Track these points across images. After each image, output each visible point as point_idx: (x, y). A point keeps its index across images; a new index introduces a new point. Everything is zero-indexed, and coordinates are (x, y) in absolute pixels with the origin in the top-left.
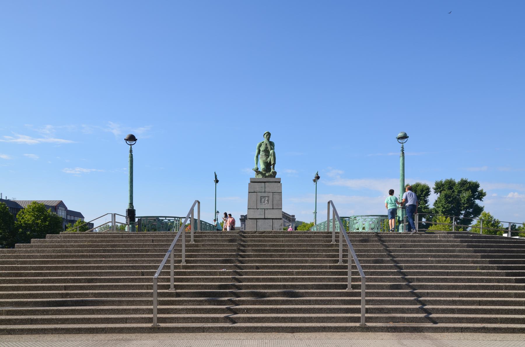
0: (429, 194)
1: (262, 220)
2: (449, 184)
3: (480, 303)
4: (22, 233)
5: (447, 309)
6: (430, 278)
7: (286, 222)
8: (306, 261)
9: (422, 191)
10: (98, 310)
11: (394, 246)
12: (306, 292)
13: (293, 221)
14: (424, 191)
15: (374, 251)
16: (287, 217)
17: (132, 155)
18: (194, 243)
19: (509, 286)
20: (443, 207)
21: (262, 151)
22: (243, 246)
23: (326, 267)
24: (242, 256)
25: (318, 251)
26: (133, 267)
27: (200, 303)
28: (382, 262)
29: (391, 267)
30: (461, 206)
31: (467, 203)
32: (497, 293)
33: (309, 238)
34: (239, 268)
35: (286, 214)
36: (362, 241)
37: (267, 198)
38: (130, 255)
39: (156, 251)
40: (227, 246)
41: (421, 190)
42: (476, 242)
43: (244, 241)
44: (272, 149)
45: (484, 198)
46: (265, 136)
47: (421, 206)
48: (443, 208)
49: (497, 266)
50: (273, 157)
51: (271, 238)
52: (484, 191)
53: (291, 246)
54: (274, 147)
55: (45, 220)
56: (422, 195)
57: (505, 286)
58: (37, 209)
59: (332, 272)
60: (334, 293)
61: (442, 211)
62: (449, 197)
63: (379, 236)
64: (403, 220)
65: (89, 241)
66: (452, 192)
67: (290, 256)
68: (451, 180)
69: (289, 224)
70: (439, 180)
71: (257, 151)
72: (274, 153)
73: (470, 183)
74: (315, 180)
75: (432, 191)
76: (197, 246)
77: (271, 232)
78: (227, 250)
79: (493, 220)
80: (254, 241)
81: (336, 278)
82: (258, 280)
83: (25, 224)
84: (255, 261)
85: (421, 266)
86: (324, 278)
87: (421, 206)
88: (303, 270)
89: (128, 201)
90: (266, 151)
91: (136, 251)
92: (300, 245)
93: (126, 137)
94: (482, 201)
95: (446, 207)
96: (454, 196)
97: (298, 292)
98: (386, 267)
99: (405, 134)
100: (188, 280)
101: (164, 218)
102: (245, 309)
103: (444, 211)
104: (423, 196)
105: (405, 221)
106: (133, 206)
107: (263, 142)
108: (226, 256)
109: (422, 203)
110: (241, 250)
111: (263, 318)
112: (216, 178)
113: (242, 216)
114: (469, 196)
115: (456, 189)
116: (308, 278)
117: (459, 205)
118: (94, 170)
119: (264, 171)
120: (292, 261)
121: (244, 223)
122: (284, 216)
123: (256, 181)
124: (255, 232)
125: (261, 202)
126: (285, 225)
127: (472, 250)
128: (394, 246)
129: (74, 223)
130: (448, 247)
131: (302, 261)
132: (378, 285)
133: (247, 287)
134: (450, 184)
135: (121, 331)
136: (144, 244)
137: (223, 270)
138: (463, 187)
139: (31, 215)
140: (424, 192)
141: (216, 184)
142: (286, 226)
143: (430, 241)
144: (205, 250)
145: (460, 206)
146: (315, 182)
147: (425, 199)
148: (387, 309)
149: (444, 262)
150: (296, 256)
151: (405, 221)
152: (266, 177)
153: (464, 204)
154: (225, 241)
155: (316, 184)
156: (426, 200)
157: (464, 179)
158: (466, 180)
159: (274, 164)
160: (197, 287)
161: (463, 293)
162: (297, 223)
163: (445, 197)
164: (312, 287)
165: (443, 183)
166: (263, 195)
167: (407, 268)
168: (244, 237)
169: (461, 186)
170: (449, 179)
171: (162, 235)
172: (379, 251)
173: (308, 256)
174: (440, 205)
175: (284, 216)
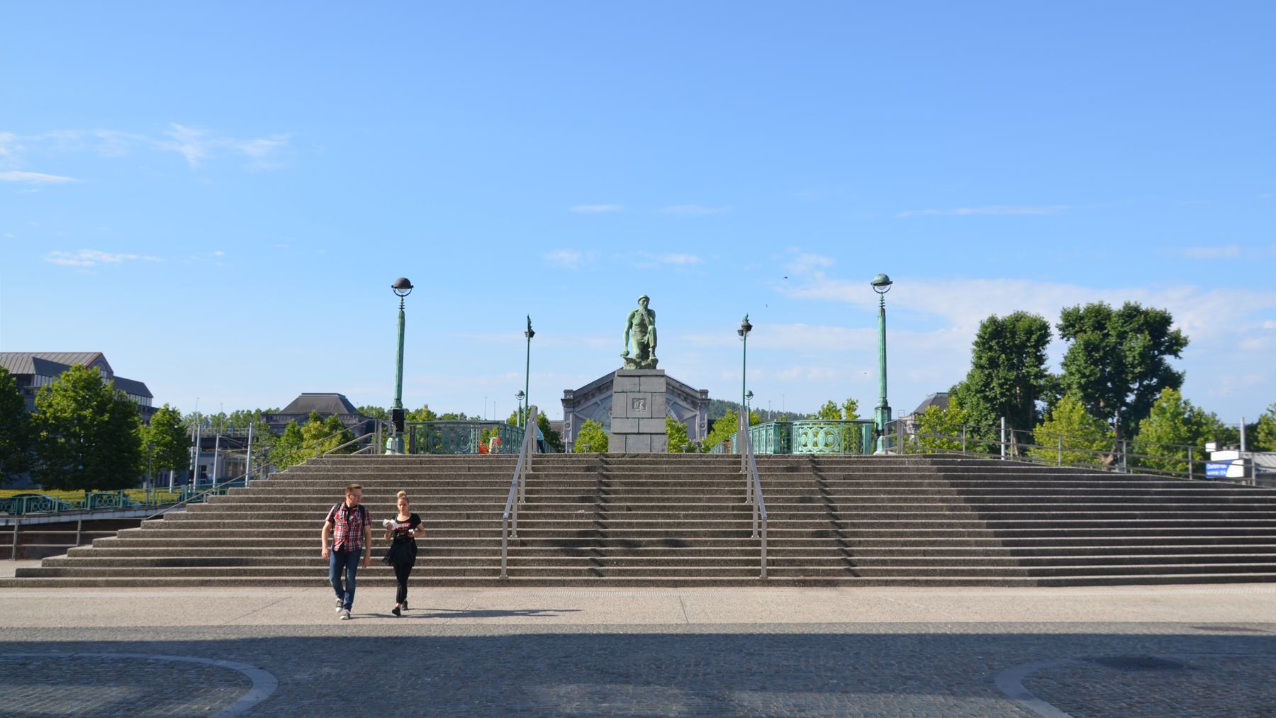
0: (1048, 342)
1: (635, 436)
2: (1096, 316)
3: (925, 553)
4: (47, 440)
5: (877, 560)
6: (870, 523)
7: (685, 408)
8: (700, 500)
9: (1029, 332)
10: (425, 560)
11: (834, 477)
12: (695, 541)
13: (703, 406)
14: (1033, 334)
15: (802, 485)
16: (687, 394)
17: (403, 313)
18: (531, 472)
19: (972, 532)
20: (1082, 374)
21: (636, 325)
22: (607, 477)
23: (727, 508)
24: (605, 492)
25: (718, 484)
26: (451, 508)
27: (555, 553)
28: (811, 500)
29: (821, 508)
30: (1127, 370)
31: (1139, 364)
32: (953, 540)
33: (708, 464)
34: (603, 508)
35: (683, 386)
36: (788, 469)
37: (642, 402)
38: (442, 490)
39: (477, 484)
40: (583, 476)
41: (1028, 330)
42: (963, 470)
43: (607, 470)
44: (652, 323)
45: (1184, 352)
46: (641, 302)
47: (1027, 372)
48: (1082, 377)
49: (972, 506)
50: (652, 337)
51: (649, 464)
52: (1183, 335)
53: (679, 477)
54: (654, 318)
55: (100, 410)
56: (1030, 342)
57: (969, 532)
58: (83, 383)
59: (734, 514)
60: (733, 542)
61: (1079, 383)
62: (1096, 349)
63: (814, 462)
64: (883, 430)
65: (373, 470)
66: (1101, 337)
67: (676, 492)
68: (1100, 305)
69: (694, 414)
70: (1070, 305)
71: (627, 324)
72: (654, 330)
73: (1146, 313)
74: (742, 331)
75: (1055, 332)
76: (537, 477)
77: (648, 456)
78: (583, 484)
79: (1189, 409)
80: (623, 469)
81: (739, 523)
82: (630, 525)
83: (56, 418)
84: (625, 500)
85: (863, 506)
86: (722, 523)
87: (1028, 372)
88: (694, 512)
89: (394, 395)
90: (643, 327)
91: (448, 484)
92: (693, 475)
93: (395, 281)
94: (1180, 358)
95: (1087, 374)
96: (1107, 346)
97: (685, 541)
98: (813, 508)
99: (887, 278)
100: (533, 525)
101: (456, 425)
102: (614, 560)
103: (1083, 383)
104: (1032, 346)
105: (886, 431)
106: (401, 403)
107: (637, 311)
108: (582, 492)
109: (1031, 364)
110: (604, 482)
111: (638, 570)
112: (529, 327)
113: (566, 392)
114: (1144, 345)
115: (1113, 328)
116: (700, 522)
117: (1120, 369)
118: (133, 257)
119: (638, 358)
120: (679, 500)
121: (572, 410)
122: (679, 392)
123: (626, 374)
124: (623, 456)
125: (633, 408)
126: (683, 417)
127: (947, 483)
128: (834, 477)
129: (150, 415)
130: (915, 479)
131: (693, 500)
132: (795, 532)
133: (616, 534)
134: (1099, 317)
135: (461, 584)
136: (458, 475)
137: (580, 512)
138: (1131, 323)
139: (71, 397)
140: (1034, 337)
141: (529, 341)
142: (685, 418)
143: (892, 470)
144: (550, 482)
145: (1123, 372)
146: (742, 335)
147: (1038, 354)
148: (800, 560)
149: (900, 500)
150: (685, 492)
151: (886, 431)
152: (641, 368)
153: (1133, 366)
154: (579, 469)
155: (745, 339)
156: (1042, 355)
157: (1132, 304)
158: (1138, 307)
159: (654, 348)
160: (547, 534)
161: (907, 541)
162: (718, 407)
163: (1086, 348)
164: (705, 534)
165: (1081, 312)
166: (637, 396)
167: (843, 508)
168: (607, 463)
169: (1126, 322)
170: (1096, 302)
171: (482, 461)
172: (810, 485)
173: (703, 492)
174: (1073, 369)
175: (679, 392)
